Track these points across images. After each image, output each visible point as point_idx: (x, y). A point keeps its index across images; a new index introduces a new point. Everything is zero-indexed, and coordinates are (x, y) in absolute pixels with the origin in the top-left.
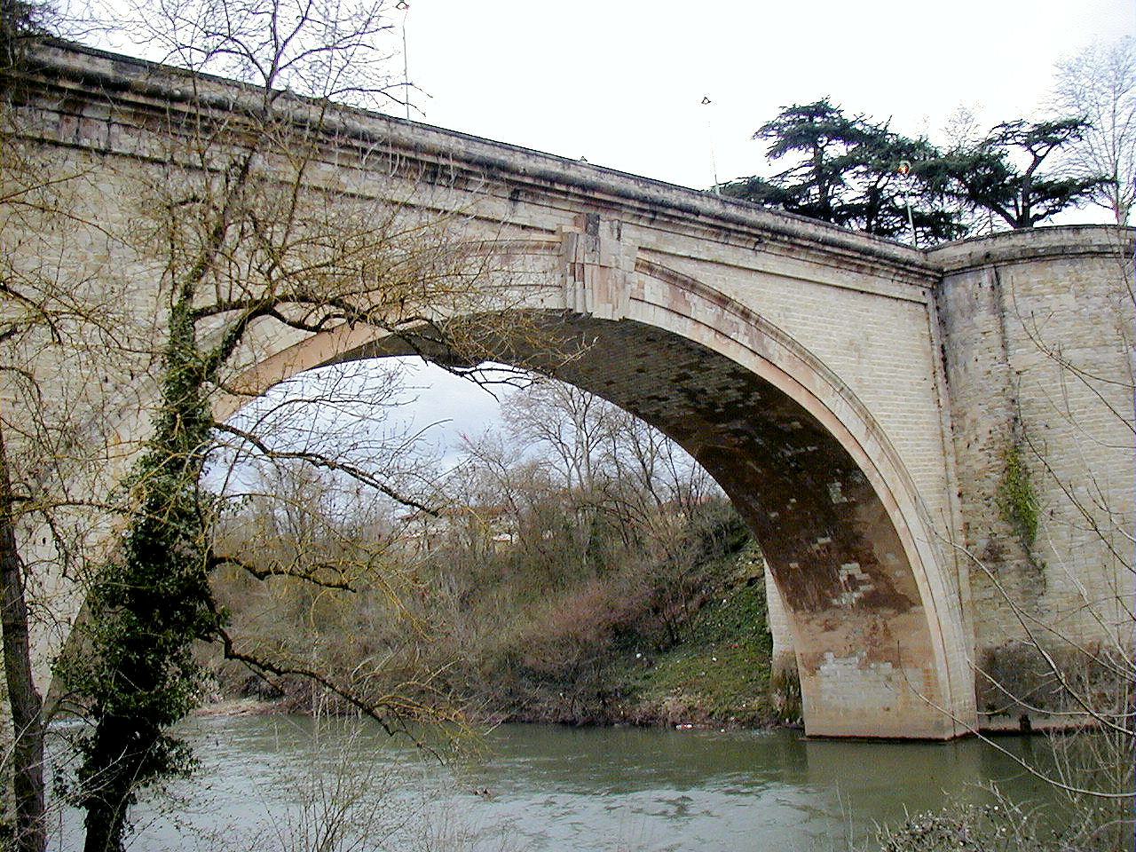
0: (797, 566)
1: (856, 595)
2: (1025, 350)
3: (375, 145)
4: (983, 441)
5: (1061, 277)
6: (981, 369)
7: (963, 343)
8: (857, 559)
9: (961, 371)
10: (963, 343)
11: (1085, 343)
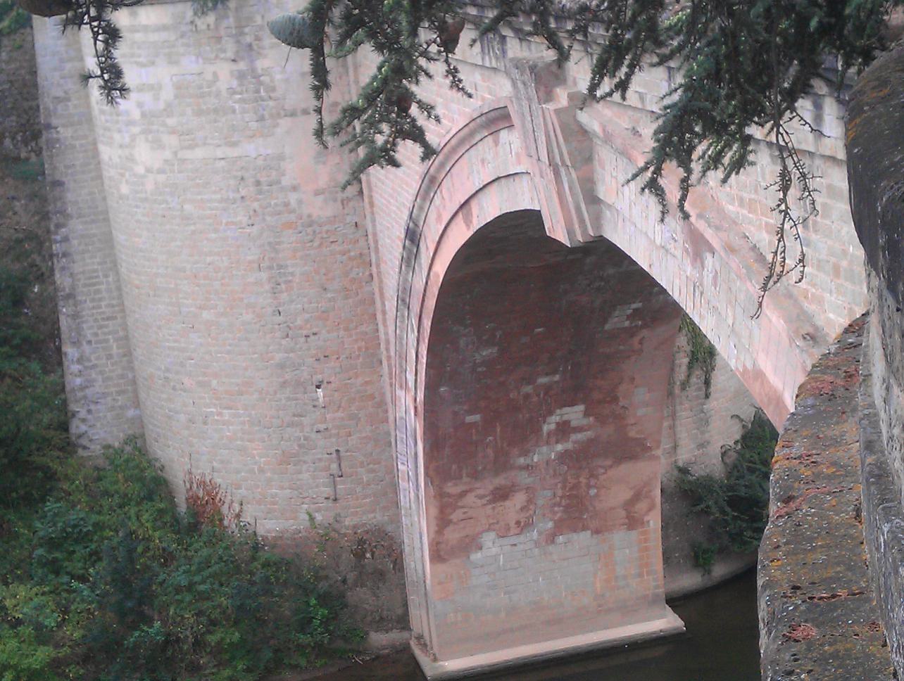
1: (559, 447)
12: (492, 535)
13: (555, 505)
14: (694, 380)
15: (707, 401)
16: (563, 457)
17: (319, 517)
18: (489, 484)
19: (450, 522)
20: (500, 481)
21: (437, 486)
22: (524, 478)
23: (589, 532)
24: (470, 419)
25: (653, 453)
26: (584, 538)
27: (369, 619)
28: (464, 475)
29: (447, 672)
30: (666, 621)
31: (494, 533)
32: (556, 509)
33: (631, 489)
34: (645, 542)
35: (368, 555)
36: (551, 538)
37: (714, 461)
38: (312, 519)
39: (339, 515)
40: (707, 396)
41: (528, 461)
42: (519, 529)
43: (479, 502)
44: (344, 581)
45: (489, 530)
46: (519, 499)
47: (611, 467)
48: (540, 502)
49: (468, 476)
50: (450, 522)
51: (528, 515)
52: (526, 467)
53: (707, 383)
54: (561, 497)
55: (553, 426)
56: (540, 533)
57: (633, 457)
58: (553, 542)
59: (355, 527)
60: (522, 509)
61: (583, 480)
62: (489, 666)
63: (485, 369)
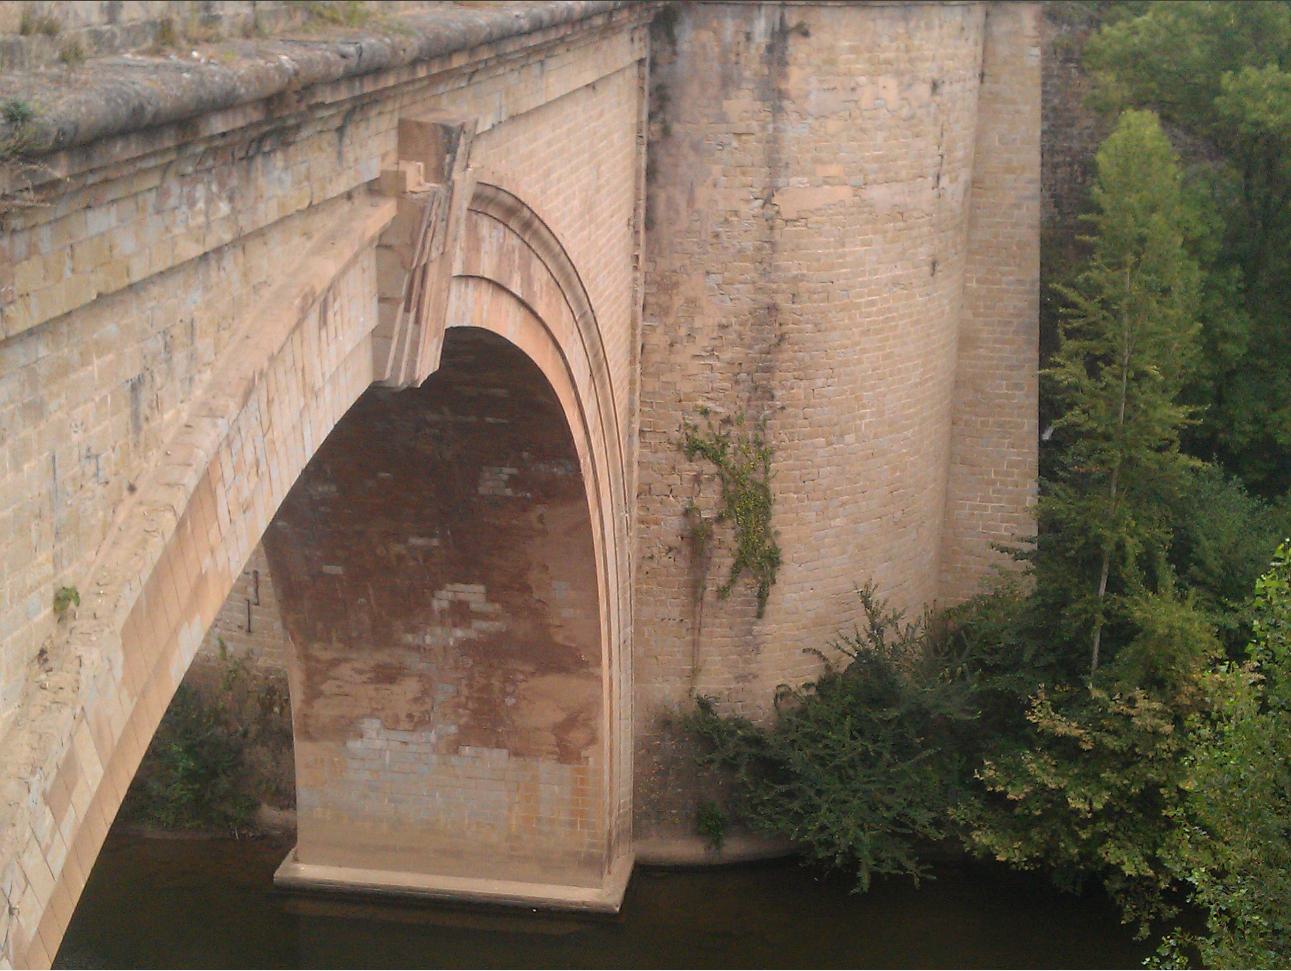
0: (341, 572)
1: (459, 633)
2: (805, 180)
3: (888, 756)
4: (703, 342)
5: (885, 42)
6: (722, 205)
7: (695, 148)
8: (482, 580)
9: (681, 200)
10: (695, 148)
11: (896, 173)
12: (376, 724)
13: (458, 706)
14: (740, 588)
15: (759, 622)
16: (465, 646)
17: (230, 648)
18: (368, 658)
19: (321, 694)
20: (383, 656)
21: (301, 644)
22: (414, 661)
23: (505, 752)
24: (329, 569)
25: (591, 670)
26: (498, 757)
27: (264, 787)
28: (334, 638)
29: (297, 879)
30: (604, 892)
31: (379, 721)
32: (461, 710)
33: (563, 709)
34: (582, 784)
35: (276, 709)
36: (455, 747)
37: (761, 702)
38: (223, 648)
39: (252, 651)
40: (760, 615)
41: (418, 641)
42: (413, 724)
43: (359, 678)
44: (245, 734)
45: (371, 716)
46: (410, 687)
47: (533, 674)
48: (440, 698)
49: (340, 640)
50: (321, 694)
51: (423, 709)
52: (418, 648)
53: (762, 597)
54: (467, 698)
55: (445, 604)
56: (440, 737)
57: (561, 669)
58: (456, 752)
59: (268, 671)
60: (416, 700)
61: (496, 683)
62: (352, 886)
63: (329, 510)
